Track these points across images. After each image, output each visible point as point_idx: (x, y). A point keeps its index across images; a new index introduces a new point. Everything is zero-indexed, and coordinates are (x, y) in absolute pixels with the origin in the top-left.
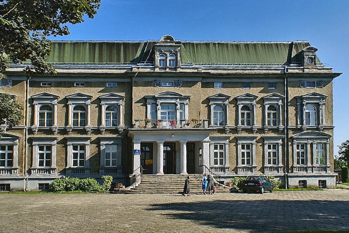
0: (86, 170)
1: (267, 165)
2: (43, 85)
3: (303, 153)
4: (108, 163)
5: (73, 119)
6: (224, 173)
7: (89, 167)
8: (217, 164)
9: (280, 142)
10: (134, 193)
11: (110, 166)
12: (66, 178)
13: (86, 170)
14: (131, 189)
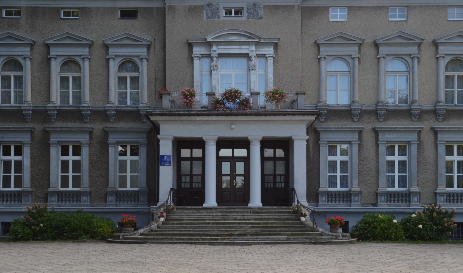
0: (380, 195)
1: (324, 187)
2: (6, 15)
3: (402, 164)
4: (123, 183)
5: (59, 90)
6: (408, 204)
7: (88, 190)
8: (452, 186)
9: (413, 137)
10: (176, 243)
11: (126, 187)
12: (375, 219)
13: (380, 195)
14: (142, 234)
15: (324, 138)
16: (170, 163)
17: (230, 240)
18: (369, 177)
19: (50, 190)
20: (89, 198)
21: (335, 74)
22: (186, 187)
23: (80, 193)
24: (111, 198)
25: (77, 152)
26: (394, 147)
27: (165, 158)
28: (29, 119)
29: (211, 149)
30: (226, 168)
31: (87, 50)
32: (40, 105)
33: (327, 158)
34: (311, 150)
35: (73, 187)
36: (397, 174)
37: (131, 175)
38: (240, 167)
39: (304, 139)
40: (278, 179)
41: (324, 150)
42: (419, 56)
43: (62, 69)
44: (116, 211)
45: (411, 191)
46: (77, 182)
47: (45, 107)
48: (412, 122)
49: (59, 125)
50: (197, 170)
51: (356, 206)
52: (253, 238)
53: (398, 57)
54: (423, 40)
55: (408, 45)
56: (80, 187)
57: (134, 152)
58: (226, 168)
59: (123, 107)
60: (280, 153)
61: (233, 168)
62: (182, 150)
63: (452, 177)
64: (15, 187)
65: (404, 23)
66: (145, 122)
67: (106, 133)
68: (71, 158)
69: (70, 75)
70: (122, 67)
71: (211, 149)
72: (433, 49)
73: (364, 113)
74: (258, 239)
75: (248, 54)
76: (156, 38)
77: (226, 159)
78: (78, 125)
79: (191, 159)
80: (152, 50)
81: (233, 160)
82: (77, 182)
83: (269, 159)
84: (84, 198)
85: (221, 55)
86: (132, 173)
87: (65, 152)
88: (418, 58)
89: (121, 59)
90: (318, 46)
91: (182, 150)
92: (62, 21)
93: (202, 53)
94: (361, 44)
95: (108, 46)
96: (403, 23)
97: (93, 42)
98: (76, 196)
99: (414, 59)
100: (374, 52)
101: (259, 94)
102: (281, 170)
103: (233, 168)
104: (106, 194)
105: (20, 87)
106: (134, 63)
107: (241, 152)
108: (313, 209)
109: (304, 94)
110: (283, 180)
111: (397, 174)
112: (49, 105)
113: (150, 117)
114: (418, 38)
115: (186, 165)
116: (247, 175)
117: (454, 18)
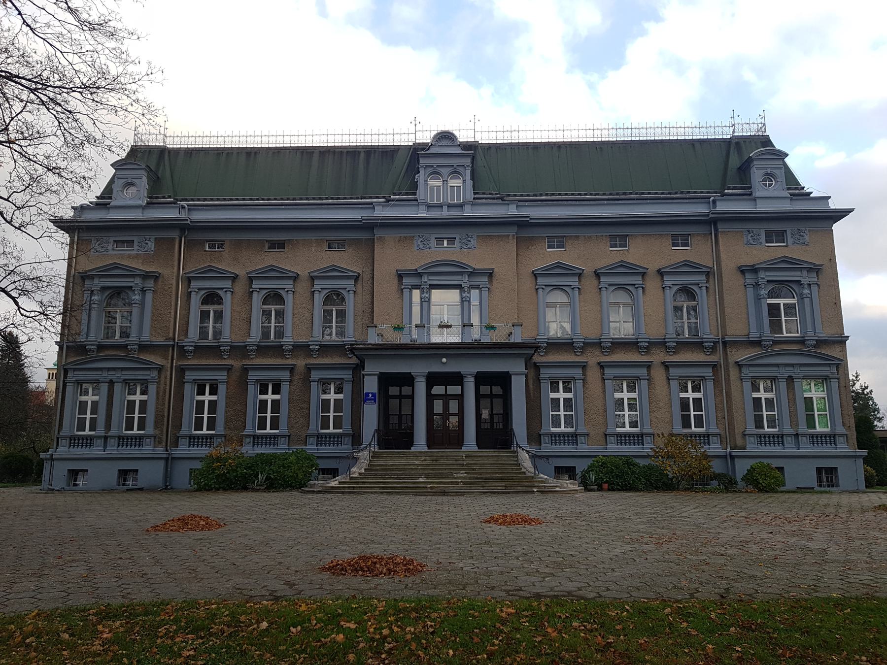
1: (188, 428)
3: (143, 404)
14: (340, 483)
15: (545, 373)
16: (375, 402)
17: (441, 488)
18: (596, 417)
19: (182, 433)
20: (287, 440)
21: (553, 305)
22: (498, 427)
26: (558, 383)
27: (370, 395)
28: (227, 355)
29: (420, 387)
30: (438, 407)
31: (291, 282)
34: (531, 386)
35: (138, 430)
38: (454, 406)
39: (523, 374)
40: (495, 420)
41: (545, 386)
42: (580, 287)
43: (265, 302)
44: (141, 456)
45: (644, 432)
46: (275, 424)
47: (664, 339)
48: (640, 356)
50: (406, 410)
51: (583, 448)
52: (467, 487)
53: (621, 287)
54: (648, 269)
56: (95, 431)
57: (339, 391)
58: (438, 407)
59: (203, 342)
60: (497, 390)
61: (446, 407)
62: (391, 388)
64: (138, 430)
66: (351, 357)
67: (245, 370)
69: (273, 308)
70: (328, 300)
71: (420, 387)
72: (659, 278)
73: (587, 345)
74: (473, 488)
75: (461, 285)
76: (364, 270)
77: (438, 397)
78: (279, 361)
79: (400, 397)
80: (360, 282)
81: (446, 398)
82: (211, 425)
83: (485, 396)
86: (567, 412)
87: (264, 391)
88: (642, 287)
89: (204, 292)
90: (535, 275)
91: (391, 388)
92: (266, 254)
93: (412, 284)
94: (581, 274)
95: (85, 278)
96: (625, 251)
97: (298, 275)
98: (138, 440)
99: (602, 289)
100: (595, 282)
101: (472, 326)
102: (498, 409)
103: (446, 407)
105: (343, 321)
106: (338, 294)
107: (454, 390)
108: (534, 453)
109: (522, 325)
110: (501, 420)
112: (186, 340)
113: (354, 351)
114: (469, 266)
115: (393, 403)
116: (461, 414)
117: (773, 243)
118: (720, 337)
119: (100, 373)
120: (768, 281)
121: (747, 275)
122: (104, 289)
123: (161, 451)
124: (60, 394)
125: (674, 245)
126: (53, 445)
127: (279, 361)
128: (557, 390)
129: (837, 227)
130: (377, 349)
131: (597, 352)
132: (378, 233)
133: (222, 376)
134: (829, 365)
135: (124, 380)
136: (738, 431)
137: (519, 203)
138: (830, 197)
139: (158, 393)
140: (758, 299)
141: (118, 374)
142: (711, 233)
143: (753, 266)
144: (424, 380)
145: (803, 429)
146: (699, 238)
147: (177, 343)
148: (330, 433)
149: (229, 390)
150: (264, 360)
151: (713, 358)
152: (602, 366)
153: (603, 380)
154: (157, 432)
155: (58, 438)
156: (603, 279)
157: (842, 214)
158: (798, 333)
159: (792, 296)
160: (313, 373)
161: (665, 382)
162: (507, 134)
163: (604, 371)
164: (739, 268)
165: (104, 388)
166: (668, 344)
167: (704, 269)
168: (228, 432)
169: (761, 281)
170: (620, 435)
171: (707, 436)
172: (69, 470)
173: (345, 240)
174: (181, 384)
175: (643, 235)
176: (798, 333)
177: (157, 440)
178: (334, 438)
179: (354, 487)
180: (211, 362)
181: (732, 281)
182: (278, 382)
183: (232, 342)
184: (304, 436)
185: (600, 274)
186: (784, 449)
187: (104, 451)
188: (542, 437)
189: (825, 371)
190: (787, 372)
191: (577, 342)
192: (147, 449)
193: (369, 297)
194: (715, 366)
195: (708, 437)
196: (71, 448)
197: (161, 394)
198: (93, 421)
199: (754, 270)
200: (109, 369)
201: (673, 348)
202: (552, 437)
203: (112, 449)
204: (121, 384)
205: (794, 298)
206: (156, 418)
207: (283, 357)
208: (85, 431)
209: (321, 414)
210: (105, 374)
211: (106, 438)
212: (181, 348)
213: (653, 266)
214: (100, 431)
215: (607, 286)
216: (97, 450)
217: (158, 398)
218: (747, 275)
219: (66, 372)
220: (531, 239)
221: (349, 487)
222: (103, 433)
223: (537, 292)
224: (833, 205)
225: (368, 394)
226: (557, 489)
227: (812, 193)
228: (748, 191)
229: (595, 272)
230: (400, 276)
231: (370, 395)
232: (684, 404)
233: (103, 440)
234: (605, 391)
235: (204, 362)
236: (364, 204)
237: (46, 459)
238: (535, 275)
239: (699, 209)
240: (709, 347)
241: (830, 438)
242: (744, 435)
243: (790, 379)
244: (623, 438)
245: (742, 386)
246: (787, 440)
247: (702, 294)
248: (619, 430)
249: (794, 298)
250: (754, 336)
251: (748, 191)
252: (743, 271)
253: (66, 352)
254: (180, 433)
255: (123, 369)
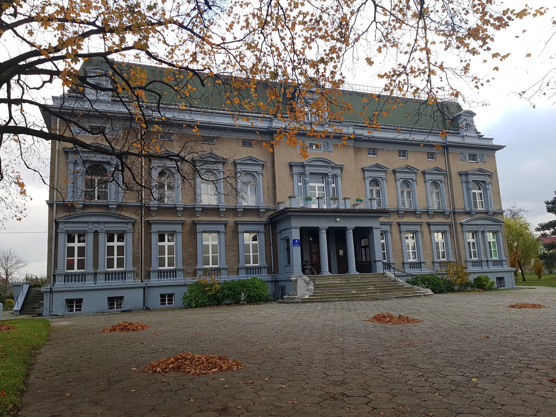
3: (121, 249)
19: (152, 269)
23: (85, 274)
24: (101, 277)
25: (121, 238)
27: (296, 241)
32: (189, 204)
33: (157, 244)
35: (78, 269)
36: (166, 256)
37: (78, 259)
41: (155, 238)
49: (203, 218)
53: (250, 173)
55: (327, 167)
63: (471, 251)
64: (78, 269)
65: (406, 160)
67: (194, 224)
68: (116, 244)
72: (422, 176)
78: (216, 219)
80: (265, 168)
82: (120, 263)
84: (89, 277)
85: (311, 174)
87: (111, 239)
90: (363, 170)
98: (173, 273)
100: (393, 176)
104: (238, 269)
111: (166, 256)
118: (452, 209)
119: (87, 225)
120: (473, 181)
121: (463, 177)
122: (84, 162)
123: (138, 282)
124: (54, 242)
125: (400, 156)
126: (50, 282)
127: (216, 219)
128: (112, 240)
129: (498, 153)
130: (301, 212)
131: (396, 216)
132: (450, 149)
133: (178, 228)
134: (498, 225)
135: (66, 231)
136: (463, 260)
137: (355, 127)
138: (493, 139)
139: (133, 240)
140: (468, 189)
141: (102, 226)
142: (444, 153)
143: (466, 172)
144: (325, 231)
145: (489, 258)
146: (439, 155)
147: (144, 204)
148: (75, 273)
149: (184, 238)
150: (206, 218)
151: (449, 221)
152: (399, 224)
153: (400, 232)
154: (135, 269)
155: (54, 276)
156: (397, 174)
157: (500, 148)
158: (483, 208)
159: (478, 188)
160: (239, 227)
161: (398, 233)
162: (369, 88)
163: (400, 227)
164: (459, 173)
165: (90, 238)
166: (261, 210)
167: (261, 163)
168: (185, 267)
169: (470, 180)
170: (247, 268)
171: (219, 270)
172: (66, 300)
173: (214, 137)
174: (149, 233)
175: (414, 151)
176: (483, 208)
177: (136, 275)
178: (253, 269)
179: (323, 298)
180: (169, 218)
181: (456, 179)
182: (122, 232)
183: (185, 205)
184: (236, 268)
185: (195, 161)
186: (483, 268)
187: (95, 284)
188: (151, 273)
189: (495, 228)
190: (481, 229)
191: (239, 208)
192: (130, 281)
193: (271, 178)
194: (450, 225)
195: (420, 264)
196: (66, 283)
197: (136, 241)
198: (255, 258)
199: (466, 174)
200: (94, 223)
201: (241, 213)
202: (158, 273)
203: (101, 282)
204: (63, 234)
205: (323, 183)
206: (133, 258)
207: (176, 215)
208: (113, 268)
209: (218, 255)
210: (91, 226)
211: (95, 274)
212: (149, 208)
213: (421, 169)
214: (89, 268)
215: (156, 167)
216: (89, 283)
217: (133, 244)
218: (463, 177)
219: (57, 223)
220: (360, 148)
221: (320, 298)
222: (92, 271)
223: (364, 180)
224: (495, 143)
225: (294, 241)
226: (427, 294)
227: (483, 136)
228: (458, 132)
229: (289, 163)
230: (291, 166)
231: (296, 241)
232: (71, 251)
233: (93, 275)
234: (401, 239)
235: (164, 218)
236: (225, 114)
237: (47, 292)
238: (363, 170)
239: (264, 125)
240: (199, 211)
241: (499, 262)
242: (466, 262)
243: (483, 232)
244: (249, 270)
245: (463, 236)
246: (484, 263)
247: (443, 186)
248: (247, 265)
249: (323, 183)
250: (468, 209)
251: (458, 132)
252: (460, 174)
253: (56, 209)
254: (151, 269)
255: (105, 223)
